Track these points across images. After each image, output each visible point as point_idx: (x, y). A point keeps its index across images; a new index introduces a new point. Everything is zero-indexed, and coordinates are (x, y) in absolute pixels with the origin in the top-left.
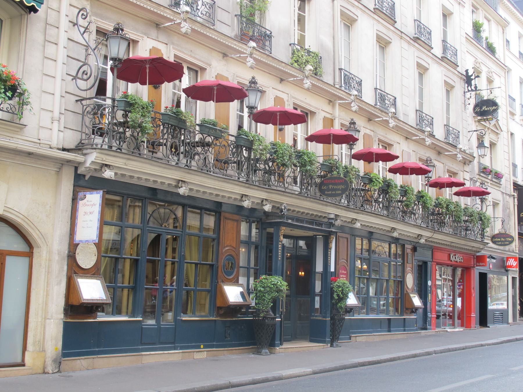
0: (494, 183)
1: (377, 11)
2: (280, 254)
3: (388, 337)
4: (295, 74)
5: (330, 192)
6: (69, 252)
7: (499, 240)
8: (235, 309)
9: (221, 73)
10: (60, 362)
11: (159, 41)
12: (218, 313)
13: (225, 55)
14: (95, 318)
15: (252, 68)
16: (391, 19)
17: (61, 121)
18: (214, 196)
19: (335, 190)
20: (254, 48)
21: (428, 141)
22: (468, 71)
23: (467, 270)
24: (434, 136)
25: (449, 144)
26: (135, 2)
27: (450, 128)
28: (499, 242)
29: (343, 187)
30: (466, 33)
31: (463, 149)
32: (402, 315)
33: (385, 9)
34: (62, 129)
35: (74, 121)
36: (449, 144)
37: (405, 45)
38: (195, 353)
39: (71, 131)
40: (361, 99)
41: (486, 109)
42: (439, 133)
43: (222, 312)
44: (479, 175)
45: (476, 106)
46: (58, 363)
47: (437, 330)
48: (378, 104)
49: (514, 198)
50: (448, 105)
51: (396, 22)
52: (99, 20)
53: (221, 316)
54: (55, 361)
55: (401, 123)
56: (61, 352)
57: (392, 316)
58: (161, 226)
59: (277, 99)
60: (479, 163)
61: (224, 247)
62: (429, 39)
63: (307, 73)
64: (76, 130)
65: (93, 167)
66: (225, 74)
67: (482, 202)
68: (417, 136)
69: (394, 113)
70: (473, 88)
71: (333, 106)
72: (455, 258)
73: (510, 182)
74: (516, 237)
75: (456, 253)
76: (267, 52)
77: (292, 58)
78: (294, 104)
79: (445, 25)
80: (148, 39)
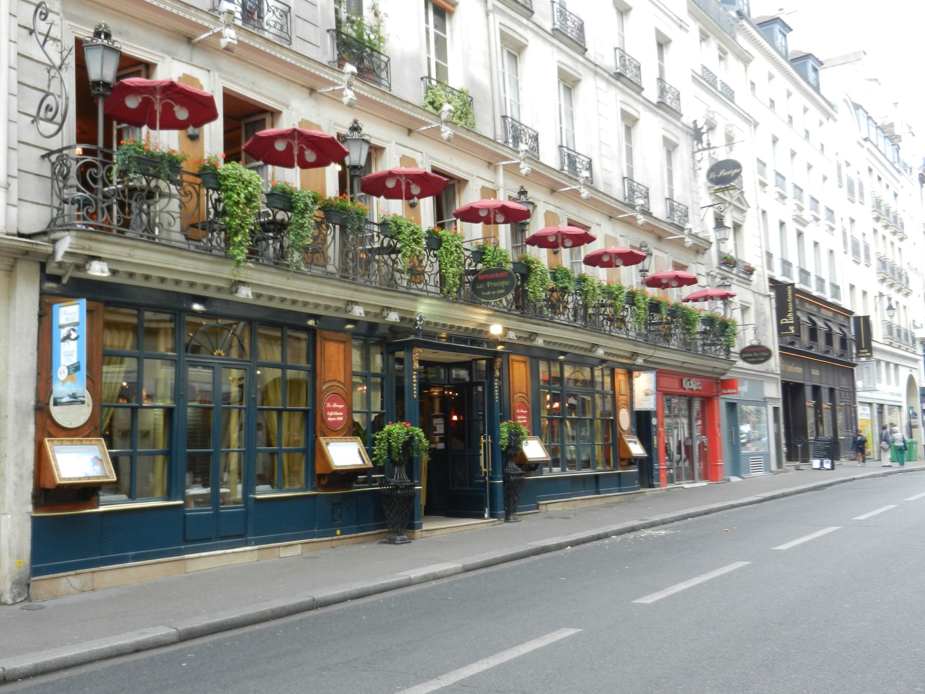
0: (742, 280)
1: (556, 32)
2: (415, 389)
3: (598, 502)
4: (427, 120)
5: (489, 293)
6: (38, 401)
7: (751, 355)
8: (349, 476)
9: (307, 118)
10: (28, 585)
11: (194, 65)
12: (319, 483)
13: (312, 91)
14: (97, 506)
15: (350, 105)
16: (579, 45)
17: (11, 188)
18: (277, 301)
19: (496, 289)
20: (353, 74)
21: (641, 219)
22: (697, 122)
23: (707, 401)
24: (651, 214)
25: (672, 224)
26: (155, 3)
27: (675, 204)
28: (750, 358)
29: (506, 283)
30: (692, 70)
31: (694, 231)
32: (615, 468)
33: (569, 31)
34: (14, 200)
35: (38, 189)
36: (672, 224)
37: (602, 85)
38: (281, 548)
39: (35, 206)
40: (473, 129)
41: (725, 174)
42: (659, 209)
43: (323, 482)
44: (720, 269)
45: (711, 170)
46: (24, 586)
47: (670, 486)
48: (566, 168)
49: (771, 299)
50: (670, 172)
51: (643, 89)
52: (78, 26)
53: (324, 488)
54: (17, 583)
55: (601, 195)
56: (28, 567)
57: (600, 470)
58: (213, 354)
59: (404, 159)
60: (720, 253)
61: (325, 383)
62: (637, 76)
63: (444, 116)
64: (43, 205)
65: (69, 260)
66: (314, 120)
67: (725, 304)
68: (427, 124)
69: (587, 178)
70: (705, 145)
71: (495, 169)
72: (690, 384)
73: (764, 277)
74: (776, 351)
75: (691, 376)
76: (383, 89)
77: (426, 98)
78: (569, 219)
79: (661, 57)
80: (175, 62)
